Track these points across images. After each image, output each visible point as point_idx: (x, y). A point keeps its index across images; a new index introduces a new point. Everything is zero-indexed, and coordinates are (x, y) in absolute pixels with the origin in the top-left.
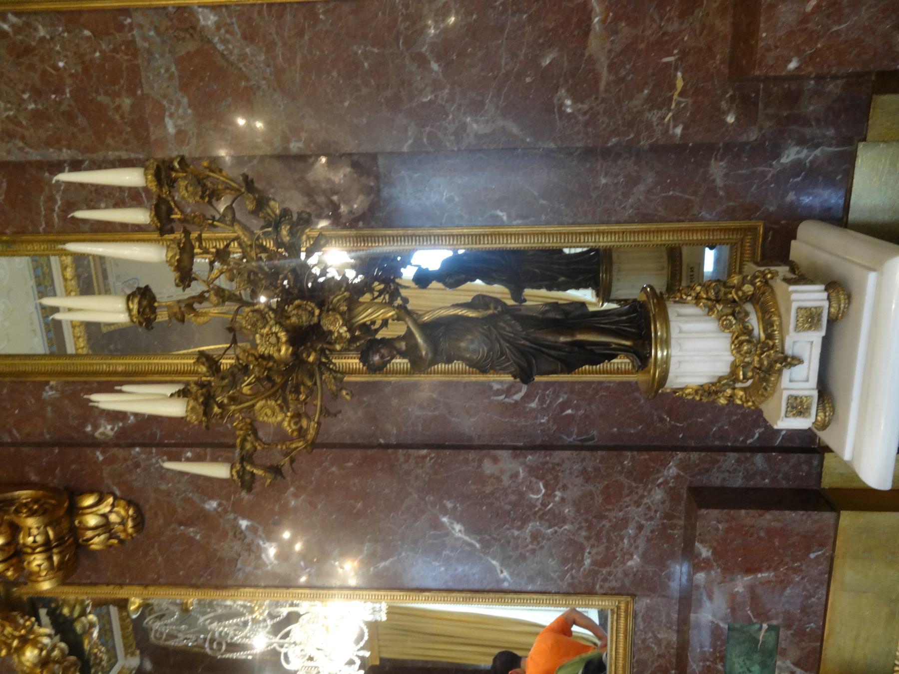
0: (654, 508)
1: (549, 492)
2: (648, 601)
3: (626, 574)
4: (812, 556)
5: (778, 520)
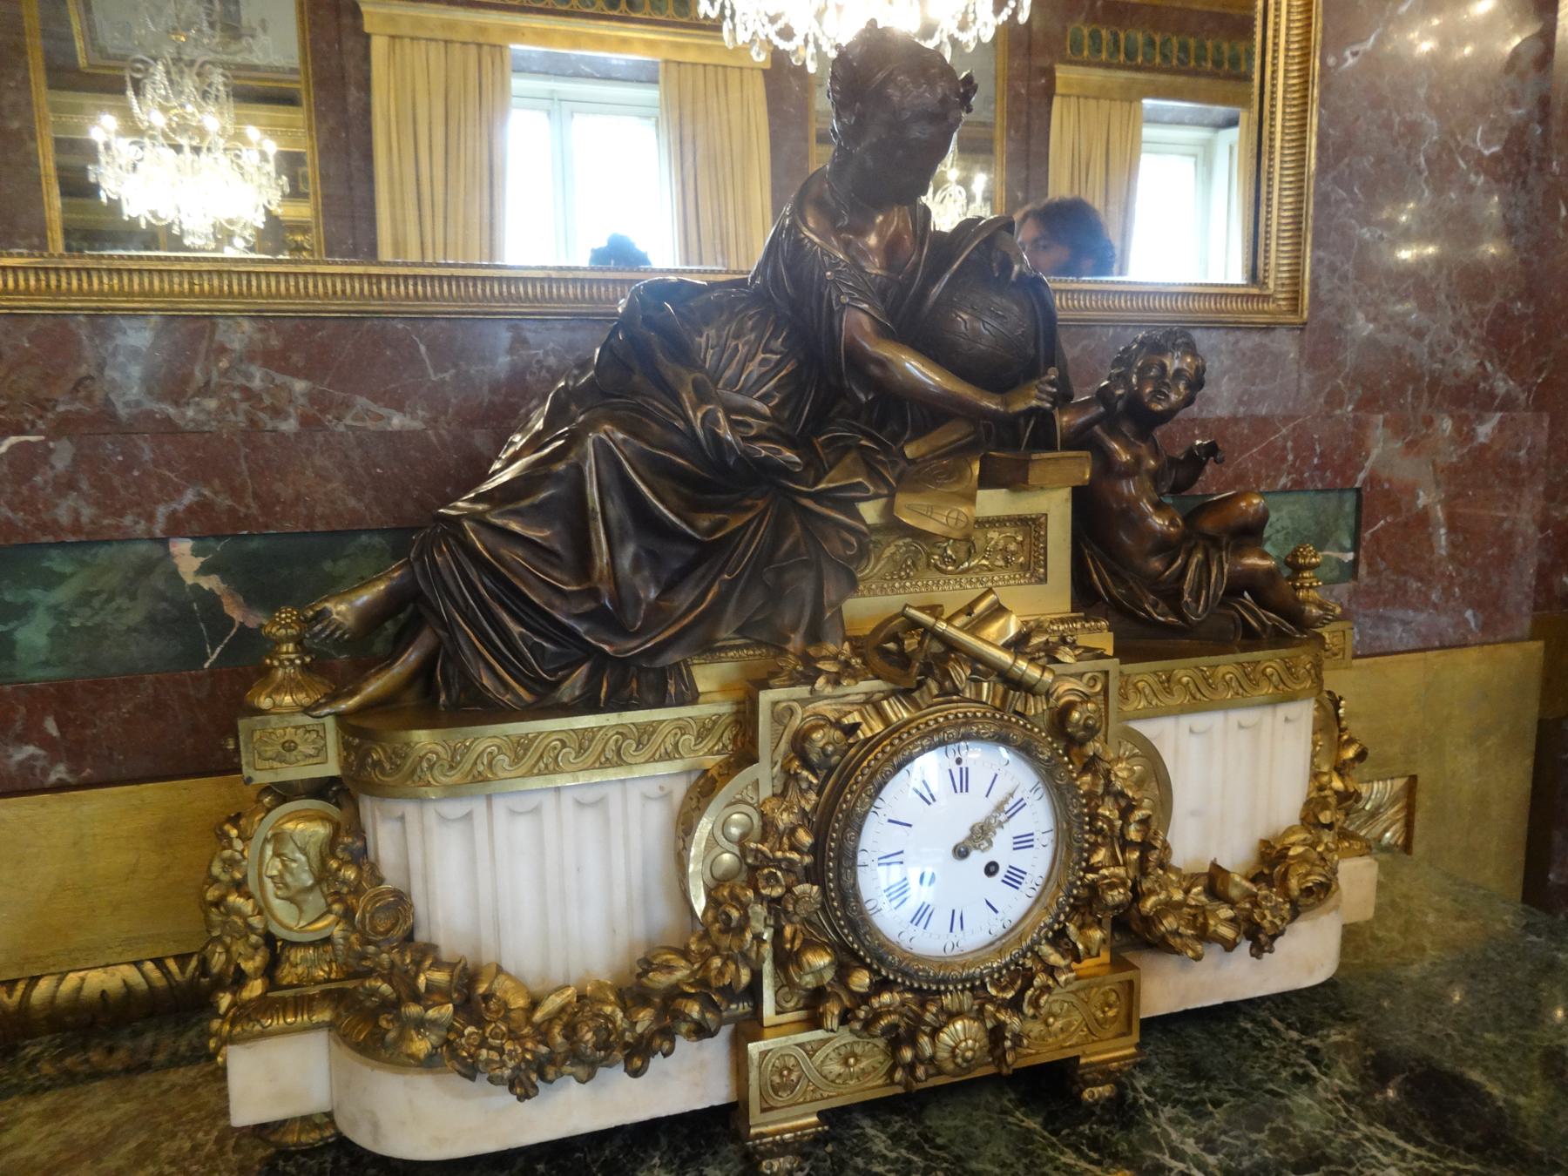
0: (1449, 357)
1: (1485, 163)
2: (1292, 355)
3: (1342, 309)
4: (1469, 614)
5: (1525, 548)
